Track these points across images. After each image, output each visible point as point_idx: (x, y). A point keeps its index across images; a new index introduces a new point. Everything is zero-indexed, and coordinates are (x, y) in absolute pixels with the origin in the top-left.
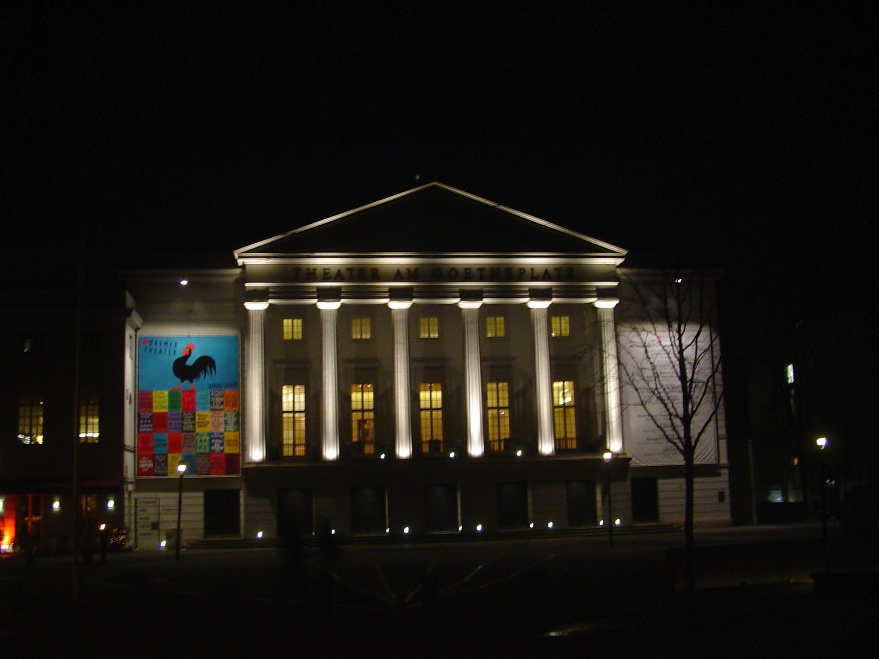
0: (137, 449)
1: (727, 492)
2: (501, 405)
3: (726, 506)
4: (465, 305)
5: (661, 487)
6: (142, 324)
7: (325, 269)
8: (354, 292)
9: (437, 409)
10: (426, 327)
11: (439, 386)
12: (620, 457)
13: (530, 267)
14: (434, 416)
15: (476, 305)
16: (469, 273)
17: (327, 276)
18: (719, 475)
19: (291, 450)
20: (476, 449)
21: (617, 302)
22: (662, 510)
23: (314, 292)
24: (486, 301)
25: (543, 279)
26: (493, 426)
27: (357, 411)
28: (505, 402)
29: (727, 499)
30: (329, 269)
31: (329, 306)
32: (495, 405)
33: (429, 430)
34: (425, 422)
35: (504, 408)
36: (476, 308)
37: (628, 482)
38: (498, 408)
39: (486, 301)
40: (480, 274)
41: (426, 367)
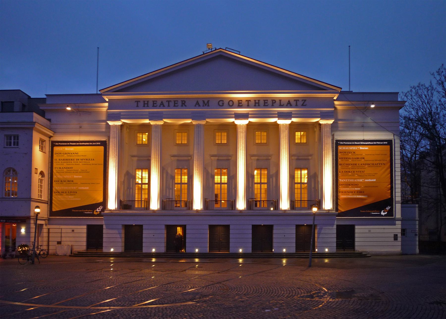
0: (49, 201)
1: (399, 235)
2: (262, 182)
3: (399, 243)
4: (281, 122)
5: (356, 231)
6: (54, 134)
7: (239, 101)
8: (128, 115)
9: (224, 183)
10: (220, 137)
11: (147, 170)
12: (330, 212)
13: (237, 100)
14: (222, 188)
15: (288, 122)
16: (241, 103)
17: (240, 105)
18: (395, 224)
19: (299, 204)
20: (285, 205)
21: (333, 120)
22: (356, 244)
23: (275, 114)
24: (295, 120)
25: (287, 106)
26: (138, 194)
27: (218, 183)
28: (265, 180)
29: (399, 239)
30: (241, 101)
31: (242, 123)
32: (259, 182)
33: (299, 195)
34: (297, 191)
35: (264, 183)
36: (330, 123)
37: (335, 227)
38: (261, 183)
39: (295, 120)
40: (248, 103)
41: (258, 160)
